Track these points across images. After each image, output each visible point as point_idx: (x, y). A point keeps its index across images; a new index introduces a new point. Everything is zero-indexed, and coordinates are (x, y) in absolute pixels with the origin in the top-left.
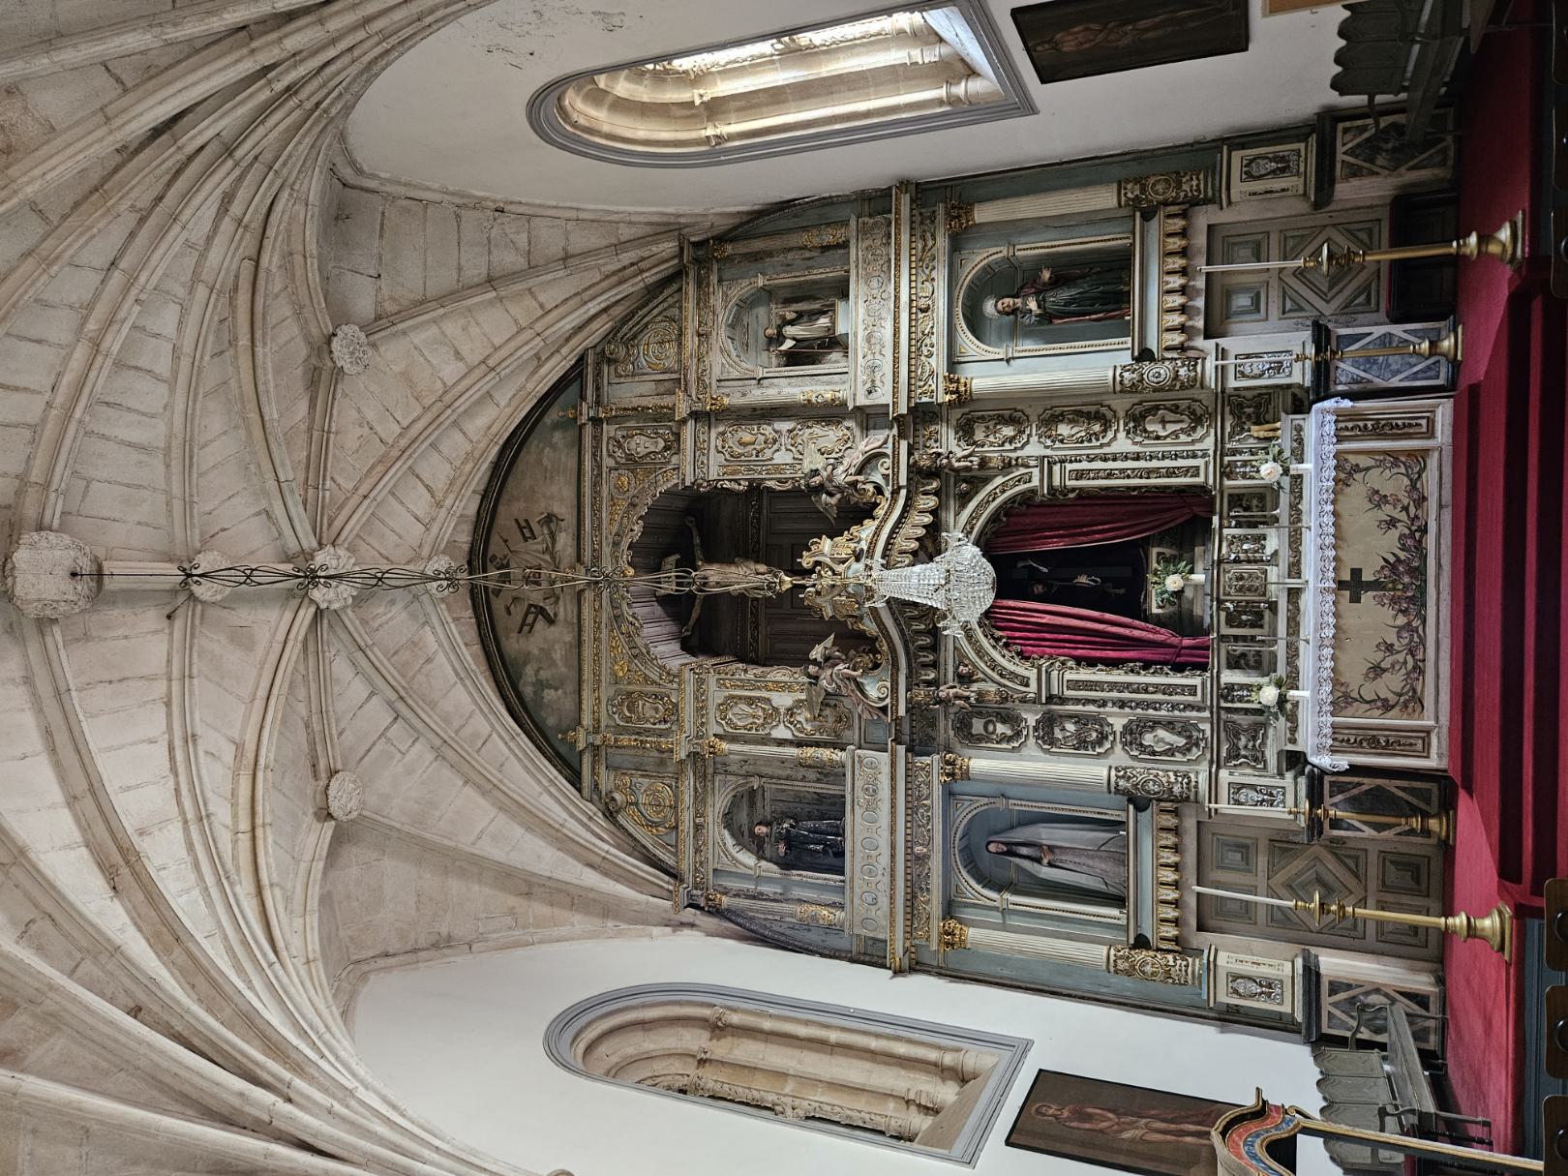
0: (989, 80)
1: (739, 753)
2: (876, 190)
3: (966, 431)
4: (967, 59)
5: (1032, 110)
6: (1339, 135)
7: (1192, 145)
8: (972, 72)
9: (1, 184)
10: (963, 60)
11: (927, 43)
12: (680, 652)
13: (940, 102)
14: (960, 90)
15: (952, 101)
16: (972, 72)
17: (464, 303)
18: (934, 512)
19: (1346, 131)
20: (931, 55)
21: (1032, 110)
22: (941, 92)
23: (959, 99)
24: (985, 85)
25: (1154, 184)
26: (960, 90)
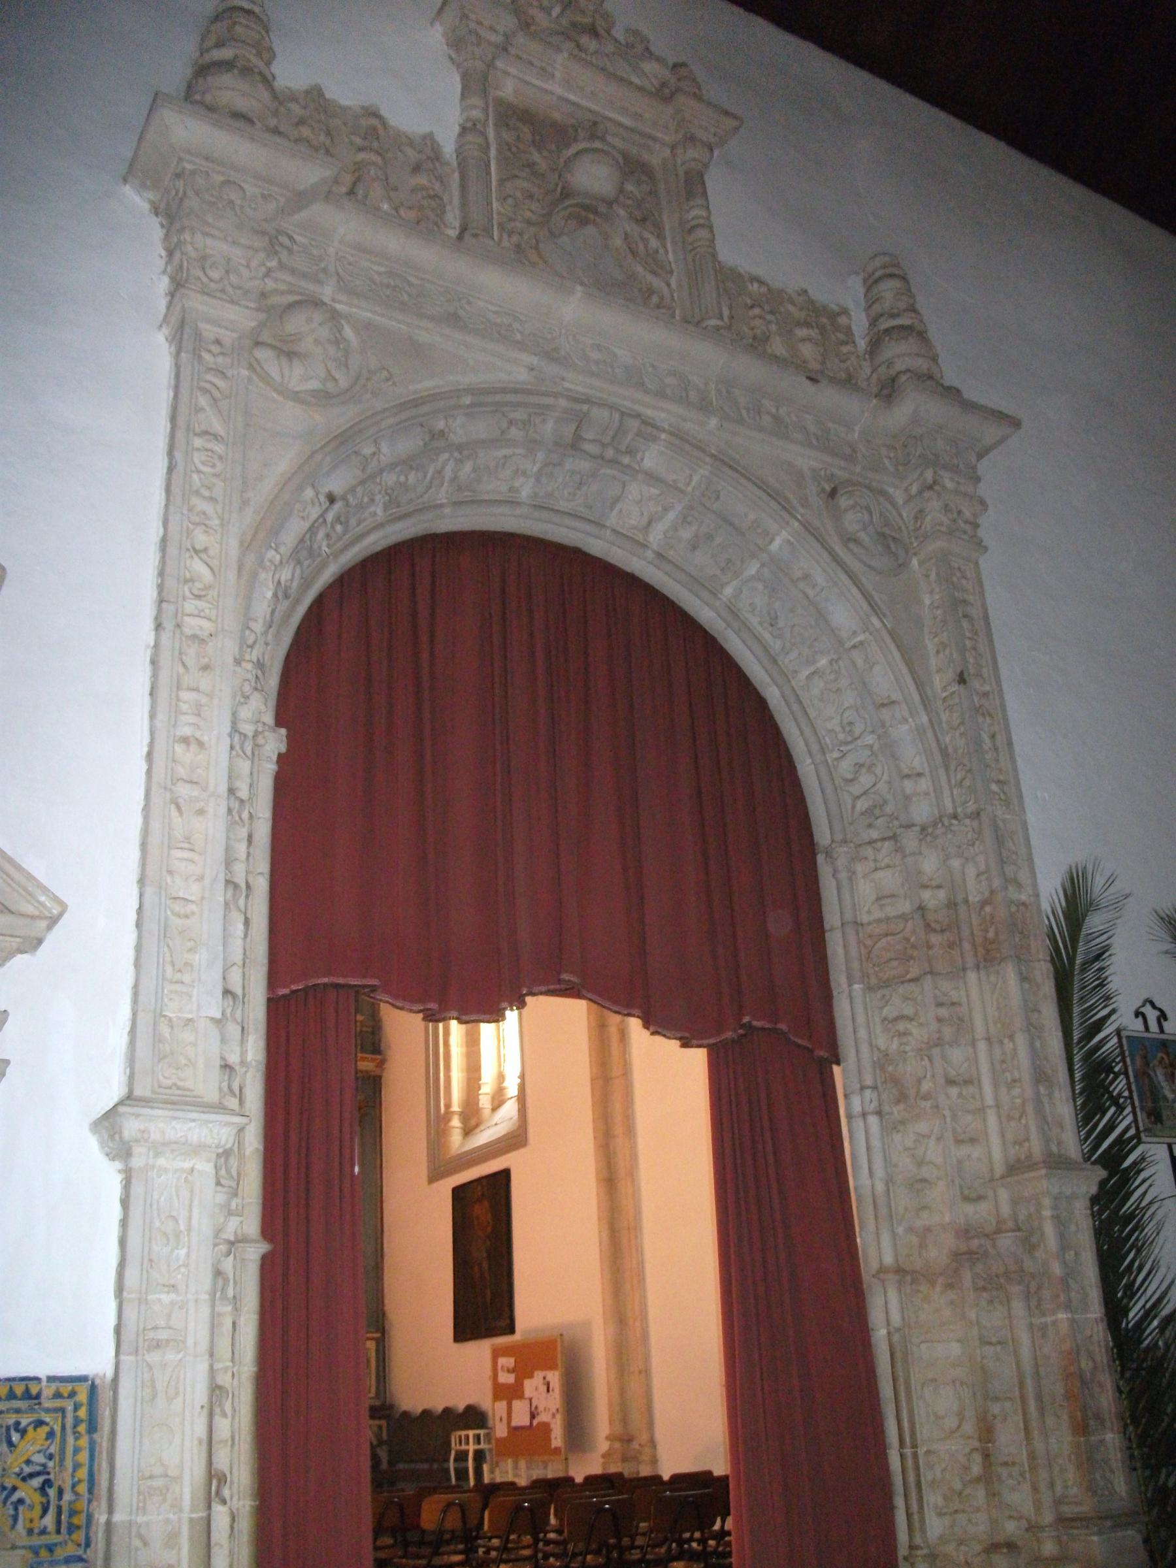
0: (462, 1145)
1: (692, 1496)
2: (380, 1041)
3: (717, 1558)
4: (478, 1130)
5: (432, 1180)
6: (377, 1422)
7: (382, 1310)
8: (468, 1132)
9: (545, 3)
10: (477, 1126)
11: (493, 1098)
12: (260, 1238)
13: (448, 1106)
14: (456, 1122)
15: (449, 1114)
16: (468, 1132)
17: (594, 107)
18: (378, 178)
19: (380, 1427)
20: (485, 1102)
21: (432, 1180)
22: (456, 1107)
23: (449, 1120)
24: (456, 1141)
25: (165, 1077)
26: (456, 1122)
